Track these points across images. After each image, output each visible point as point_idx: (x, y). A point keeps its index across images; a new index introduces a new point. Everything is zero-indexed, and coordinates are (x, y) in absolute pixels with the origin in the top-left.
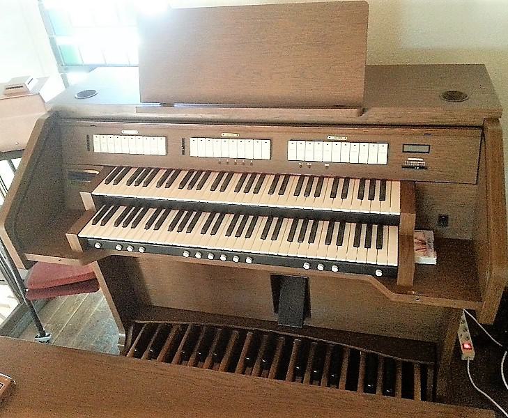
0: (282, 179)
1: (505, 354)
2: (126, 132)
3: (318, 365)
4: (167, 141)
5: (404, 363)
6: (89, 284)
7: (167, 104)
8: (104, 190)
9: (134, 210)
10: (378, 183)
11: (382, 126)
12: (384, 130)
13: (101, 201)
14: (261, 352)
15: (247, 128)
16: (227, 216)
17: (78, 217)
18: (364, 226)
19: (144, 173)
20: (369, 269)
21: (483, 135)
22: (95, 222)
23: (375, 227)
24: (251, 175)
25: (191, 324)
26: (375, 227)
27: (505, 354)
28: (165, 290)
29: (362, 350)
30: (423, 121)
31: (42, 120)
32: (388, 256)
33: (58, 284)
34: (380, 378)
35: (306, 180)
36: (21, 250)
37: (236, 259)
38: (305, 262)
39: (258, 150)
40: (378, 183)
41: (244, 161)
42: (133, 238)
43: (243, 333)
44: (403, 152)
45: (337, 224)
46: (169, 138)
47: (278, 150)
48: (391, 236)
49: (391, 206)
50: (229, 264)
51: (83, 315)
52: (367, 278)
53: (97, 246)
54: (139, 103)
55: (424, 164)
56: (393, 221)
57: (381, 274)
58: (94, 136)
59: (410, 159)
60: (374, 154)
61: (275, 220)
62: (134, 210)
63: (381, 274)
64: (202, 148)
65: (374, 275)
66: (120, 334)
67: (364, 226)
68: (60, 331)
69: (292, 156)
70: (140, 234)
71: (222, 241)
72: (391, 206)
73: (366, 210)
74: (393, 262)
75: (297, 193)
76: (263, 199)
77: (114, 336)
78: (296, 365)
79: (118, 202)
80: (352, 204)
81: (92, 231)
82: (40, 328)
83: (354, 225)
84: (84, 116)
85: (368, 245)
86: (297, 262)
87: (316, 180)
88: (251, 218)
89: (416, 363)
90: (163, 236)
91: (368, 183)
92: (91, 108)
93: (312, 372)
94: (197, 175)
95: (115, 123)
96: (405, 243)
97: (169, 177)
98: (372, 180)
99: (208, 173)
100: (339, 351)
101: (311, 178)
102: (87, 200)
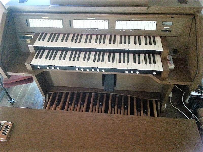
0: (66, 35)
1: (183, 95)
2: (43, 18)
3: (120, 103)
4: (63, 21)
5: (149, 100)
6: (29, 80)
7: (62, 5)
8: (38, 44)
9: (52, 51)
10: (127, 37)
11: (180, 14)
12: (156, 16)
13: (36, 48)
14: (80, 100)
15: (98, 15)
16: (59, 51)
17: (27, 55)
18: (122, 54)
19: (54, 34)
20: (151, 72)
21: (194, 17)
22: (36, 58)
23: (126, 54)
24: (101, 35)
25: (70, 92)
26: (126, 54)
27: (183, 95)
28: (59, 81)
29: (135, 97)
30: (170, 12)
31: (5, 13)
32: (158, 67)
33: (15, 81)
34: (142, 106)
35: (99, 36)
36: (5, 70)
37: (98, 71)
38: (82, 68)
39: (103, 25)
40: (127, 37)
41: (86, 30)
42: (48, 64)
43: (90, 94)
44: (162, 25)
45: (88, 53)
46: (63, 20)
47: (112, 25)
48: (158, 58)
49: (159, 47)
50: (85, 72)
51: (25, 91)
52: (150, 75)
53: (39, 68)
54: (50, 4)
55: (170, 29)
56: (159, 53)
57: (155, 74)
58: (30, 20)
59: (164, 28)
60: (151, 26)
61: (65, 52)
62: (52, 51)
63: (155, 74)
64: (78, 24)
65: (153, 74)
66: (43, 98)
67: (122, 54)
68: (17, 97)
69: (117, 27)
70: (57, 62)
71: (116, 65)
72: (159, 47)
73: (146, 49)
74: (161, 69)
75: (86, 42)
76: (59, 44)
77: (41, 98)
78: (112, 104)
79: (44, 49)
80: (143, 47)
81: (35, 62)
82: (10, 97)
83: (94, 53)
84: (24, 11)
85: (124, 62)
86: (74, 68)
87: (80, 35)
88: (55, 51)
89: (154, 101)
90: (67, 63)
91: (123, 37)
92: (27, 6)
93: (99, 104)
94: (78, 35)
95: (39, 14)
96: (164, 61)
97: (65, 37)
98: (150, 36)
99: (46, 34)
100: (126, 98)
101: (101, 36)
102: (32, 50)
